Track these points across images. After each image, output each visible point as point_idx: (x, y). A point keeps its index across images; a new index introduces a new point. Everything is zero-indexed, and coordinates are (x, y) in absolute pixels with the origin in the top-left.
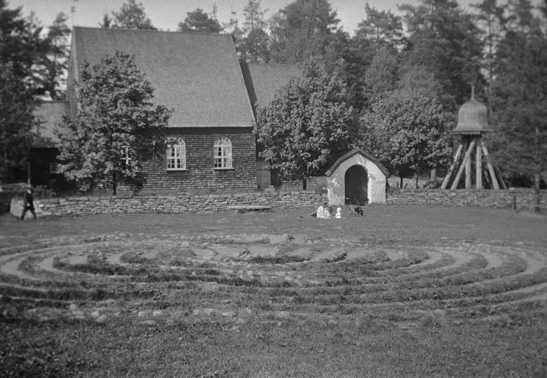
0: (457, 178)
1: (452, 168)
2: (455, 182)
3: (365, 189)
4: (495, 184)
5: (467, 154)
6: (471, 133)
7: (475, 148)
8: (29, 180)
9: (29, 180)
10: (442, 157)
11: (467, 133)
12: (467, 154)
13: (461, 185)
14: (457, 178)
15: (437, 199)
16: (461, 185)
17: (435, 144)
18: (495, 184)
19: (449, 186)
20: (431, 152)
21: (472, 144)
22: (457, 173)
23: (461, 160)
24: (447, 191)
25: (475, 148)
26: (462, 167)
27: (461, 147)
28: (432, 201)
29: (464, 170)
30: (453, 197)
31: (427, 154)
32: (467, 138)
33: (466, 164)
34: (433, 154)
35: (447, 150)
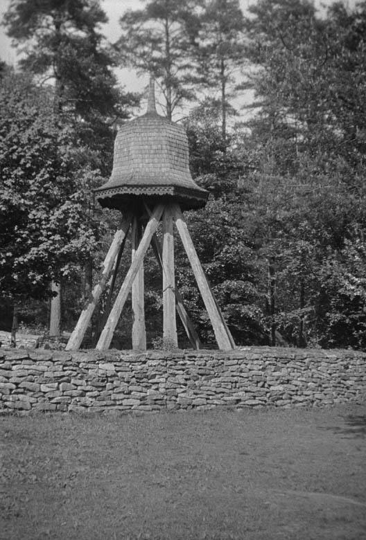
0: (113, 319)
1: (97, 291)
2: (105, 332)
3: (72, 323)
4: (221, 334)
5: (137, 254)
6: (149, 192)
7: (156, 246)
8: (197, 344)
9: (197, 344)
10: (67, 258)
11: (137, 192)
12: (137, 254)
13: (122, 341)
14: (113, 319)
15: (44, 388)
16: (122, 341)
17: (47, 220)
18: (221, 334)
19: (89, 342)
20: (37, 244)
21: (152, 225)
22: (109, 308)
23: (120, 272)
24: (83, 358)
25: (156, 246)
26: (125, 286)
27: (119, 235)
28: (27, 399)
29: (128, 304)
30: (105, 378)
31: (25, 251)
32: (135, 207)
33: (134, 284)
34: (42, 246)
35: (83, 241)
